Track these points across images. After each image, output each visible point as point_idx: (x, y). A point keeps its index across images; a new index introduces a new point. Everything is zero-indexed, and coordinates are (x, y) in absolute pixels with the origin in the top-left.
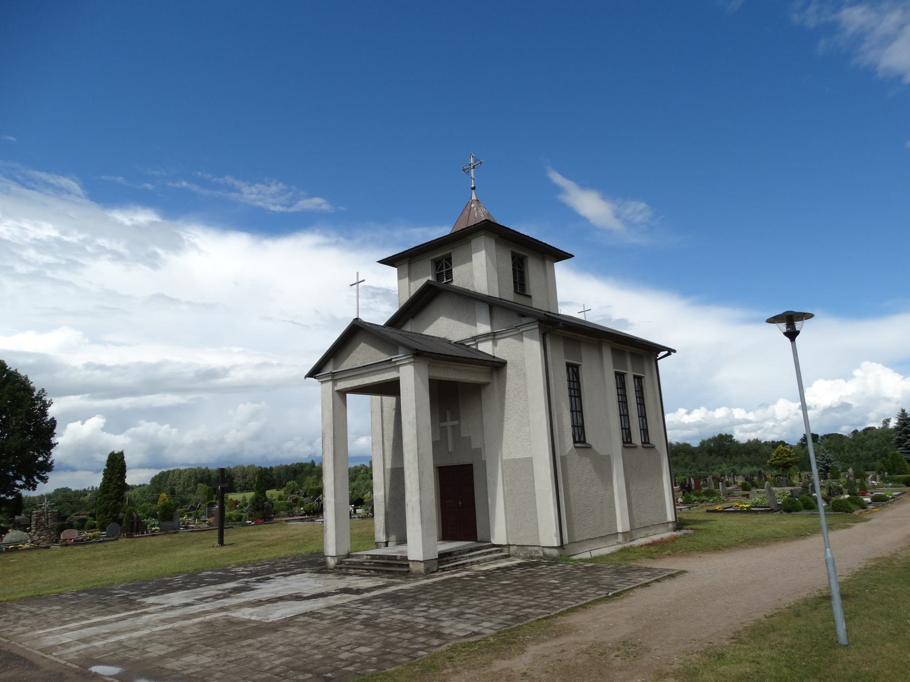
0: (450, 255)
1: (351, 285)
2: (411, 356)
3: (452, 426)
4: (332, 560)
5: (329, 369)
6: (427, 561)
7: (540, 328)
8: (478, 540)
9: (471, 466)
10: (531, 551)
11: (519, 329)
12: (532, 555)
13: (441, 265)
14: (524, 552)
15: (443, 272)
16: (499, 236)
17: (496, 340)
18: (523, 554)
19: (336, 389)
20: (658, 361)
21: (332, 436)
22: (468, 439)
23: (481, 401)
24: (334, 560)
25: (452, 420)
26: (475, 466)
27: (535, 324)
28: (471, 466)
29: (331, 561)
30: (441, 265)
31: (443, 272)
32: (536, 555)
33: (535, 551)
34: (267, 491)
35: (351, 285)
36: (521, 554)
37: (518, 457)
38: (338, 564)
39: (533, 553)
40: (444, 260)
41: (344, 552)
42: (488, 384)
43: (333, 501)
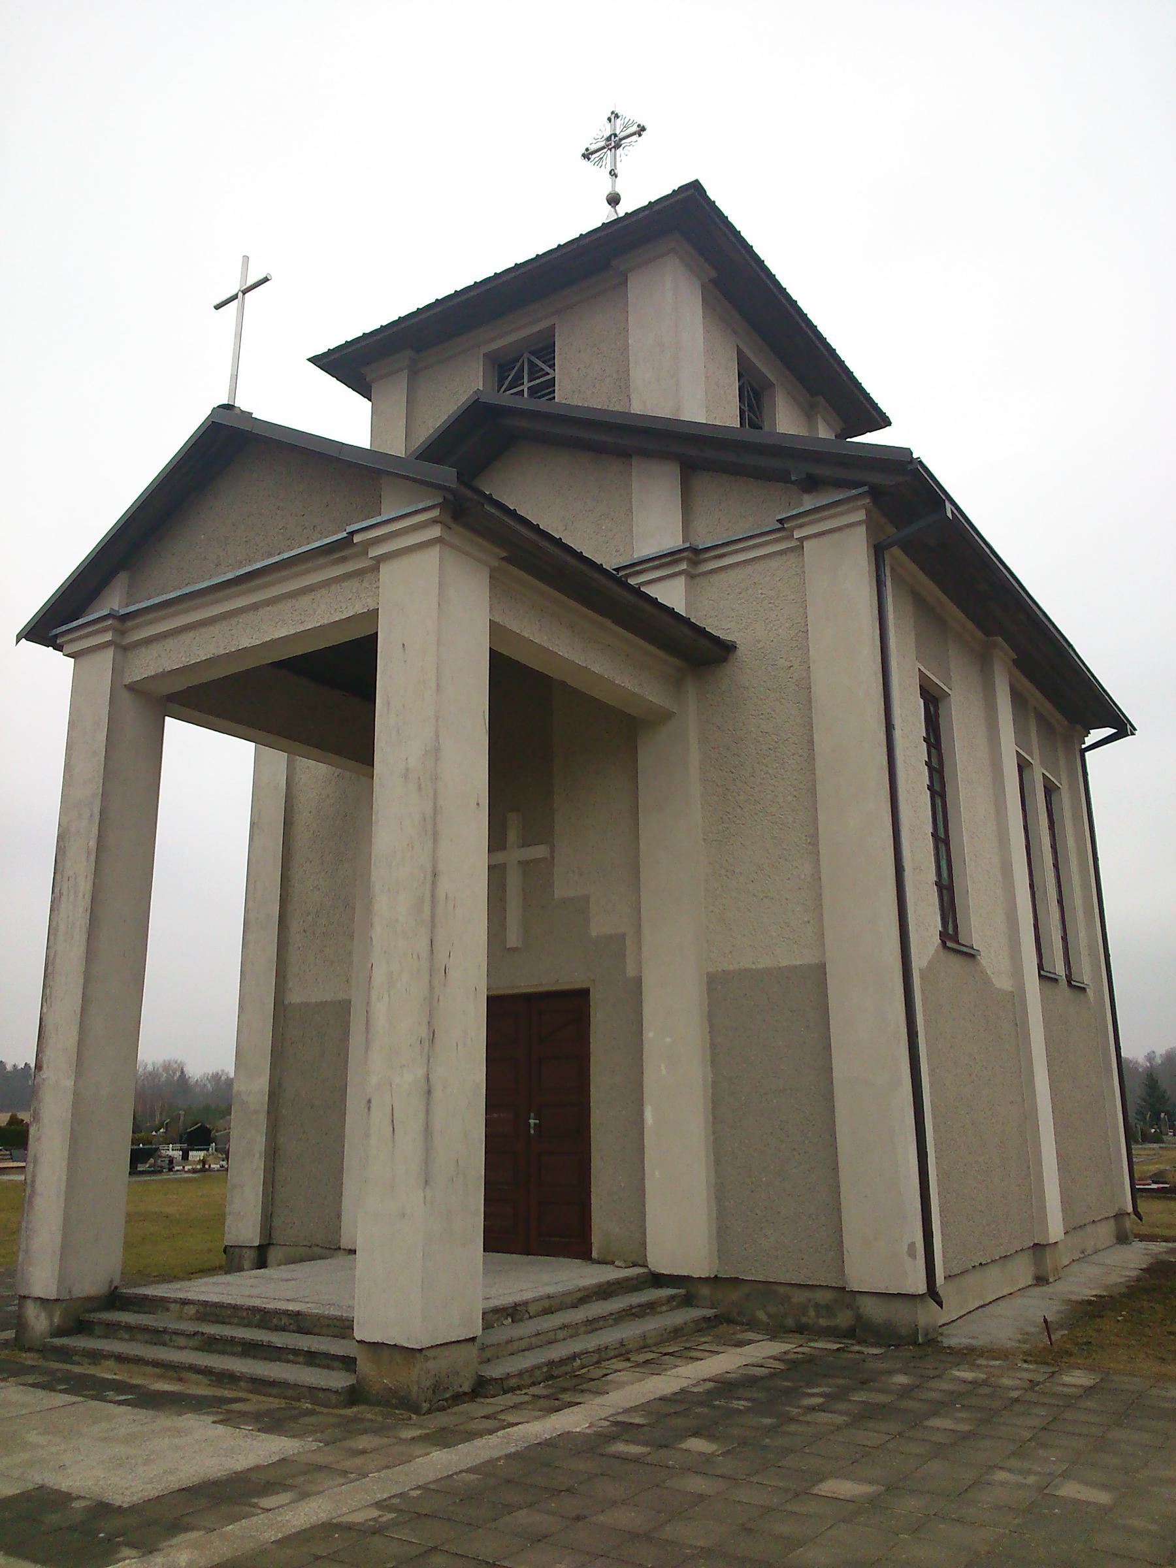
0: (550, 333)
1: (217, 307)
2: (435, 513)
3: (524, 864)
4: (43, 1315)
5: (114, 601)
6: (57, 890)
7: (871, 526)
8: (594, 1255)
9: (583, 994)
10: (804, 1309)
11: (792, 530)
12: (804, 1320)
13: (519, 364)
14: (772, 1309)
15: (530, 381)
16: (713, 274)
17: (697, 580)
18: (769, 1316)
19: (127, 681)
20: (1087, 754)
21: (93, 844)
22: (581, 906)
23: (634, 779)
24: (50, 1317)
25: (525, 844)
26: (594, 997)
27: (857, 509)
28: (583, 994)
29: (37, 1317)
30: (519, 364)
31: (530, 381)
32: (823, 1322)
33: (817, 1306)
34: (593, 1256)
35: (217, 307)
36: (761, 1315)
37: (765, 962)
38: (59, 1332)
39: (812, 1313)
40: (526, 355)
41: (90, 1285)
42: (664, 717)
43: (69, 1083)
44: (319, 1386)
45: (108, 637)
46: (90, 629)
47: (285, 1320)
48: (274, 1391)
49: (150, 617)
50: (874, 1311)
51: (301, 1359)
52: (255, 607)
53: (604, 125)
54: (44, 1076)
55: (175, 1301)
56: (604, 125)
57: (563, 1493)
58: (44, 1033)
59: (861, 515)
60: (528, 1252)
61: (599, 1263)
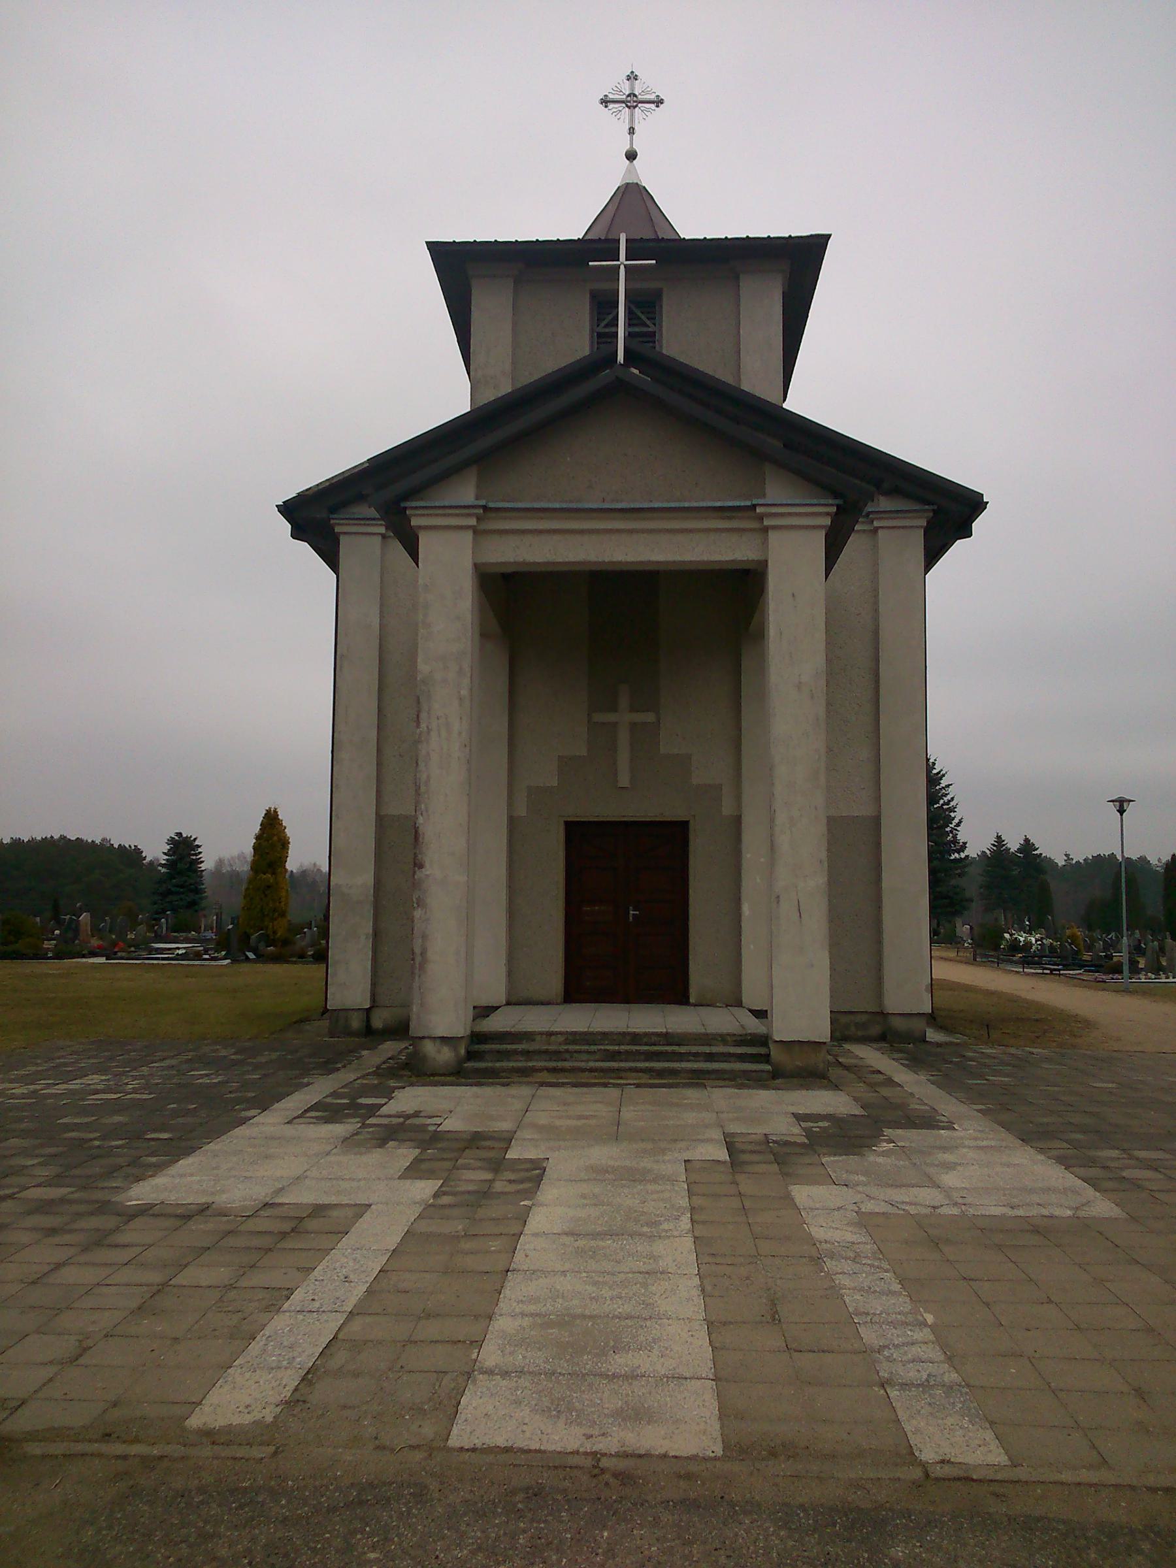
3: (633, 726)
8: (692, 1000)
25: (633, 709)
32: (860, 1033)
39: (853, 1028)
44: (753, 1070)
45: (473, 522)
46: (457, 511)
47: (654, 1039)
48: (713, 1076)
49: (508, 514)
50: (898, 1024)
51: (701, 1058)
52: (582, 532)
53: (655, 93)
54: (428, 873)
55: (541, 1034)
56: (655, 93)
57: (306, 1219)
58: (423, 838)
59: (827, 521)
60: (627, 1001)
61: (695, 1005)
